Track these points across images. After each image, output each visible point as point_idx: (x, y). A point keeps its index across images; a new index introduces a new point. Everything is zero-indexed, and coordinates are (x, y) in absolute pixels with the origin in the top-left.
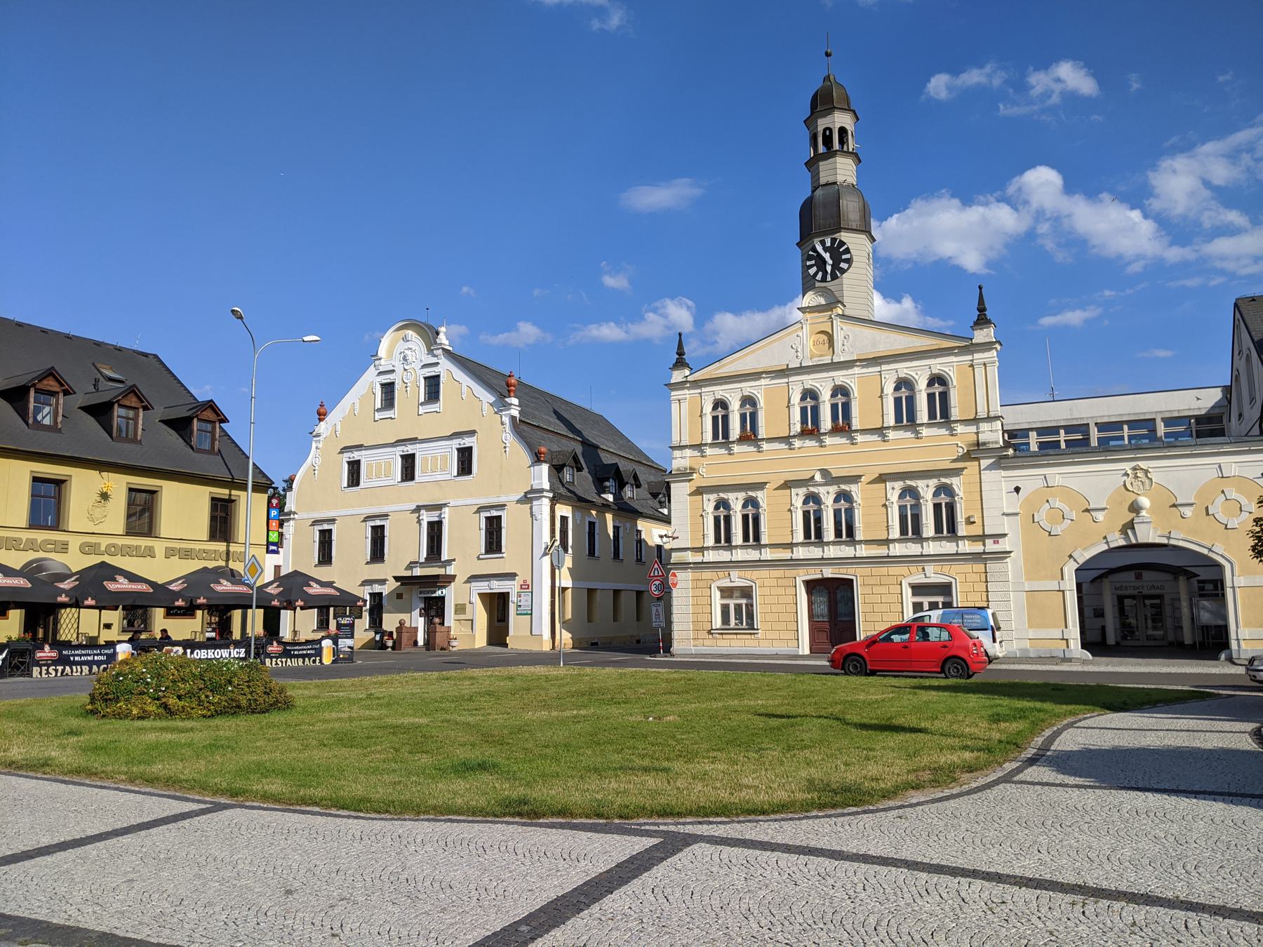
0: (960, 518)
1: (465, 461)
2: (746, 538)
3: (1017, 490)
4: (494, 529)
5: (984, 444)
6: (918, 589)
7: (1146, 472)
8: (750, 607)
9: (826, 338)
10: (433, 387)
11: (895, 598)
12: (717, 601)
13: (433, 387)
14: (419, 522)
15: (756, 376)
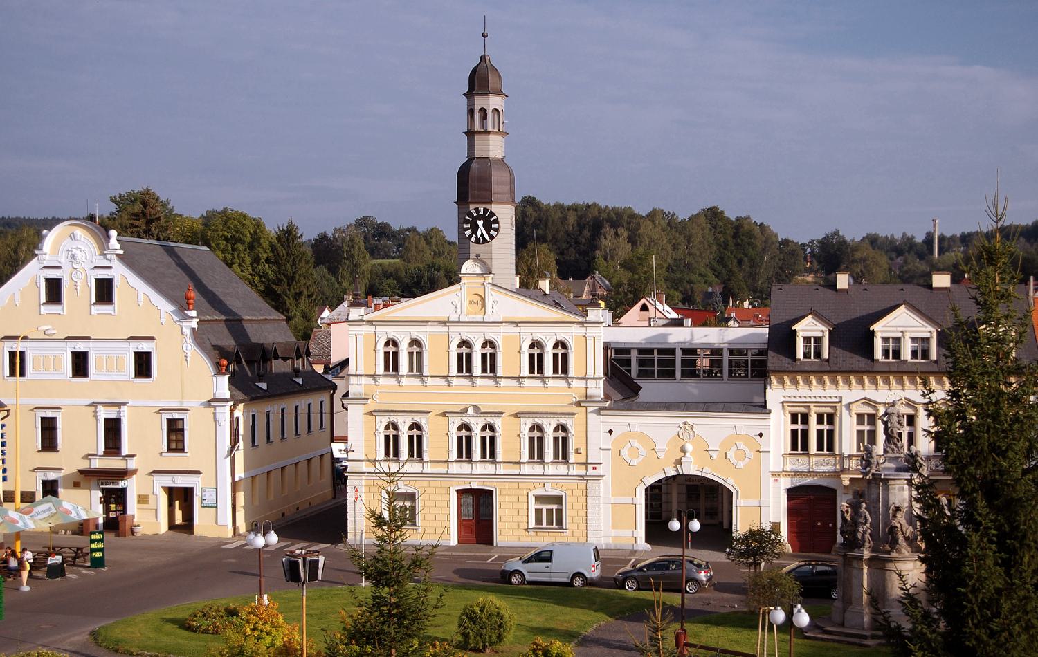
0: (571, 450)
1: (143, 365)
2: (484, 456)
3: (611, 432)
4: (175, 430)
5: (591, 397)
6: (539, 499)
7: (692, 426)
8: (560, 512)
9: (479, 299)
10: (105, 291)
11: (522, 506)
12: (533, 506)
13: (105, 291)
14: (96, 416)
15: (425, 322)
